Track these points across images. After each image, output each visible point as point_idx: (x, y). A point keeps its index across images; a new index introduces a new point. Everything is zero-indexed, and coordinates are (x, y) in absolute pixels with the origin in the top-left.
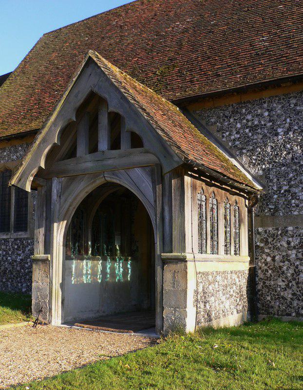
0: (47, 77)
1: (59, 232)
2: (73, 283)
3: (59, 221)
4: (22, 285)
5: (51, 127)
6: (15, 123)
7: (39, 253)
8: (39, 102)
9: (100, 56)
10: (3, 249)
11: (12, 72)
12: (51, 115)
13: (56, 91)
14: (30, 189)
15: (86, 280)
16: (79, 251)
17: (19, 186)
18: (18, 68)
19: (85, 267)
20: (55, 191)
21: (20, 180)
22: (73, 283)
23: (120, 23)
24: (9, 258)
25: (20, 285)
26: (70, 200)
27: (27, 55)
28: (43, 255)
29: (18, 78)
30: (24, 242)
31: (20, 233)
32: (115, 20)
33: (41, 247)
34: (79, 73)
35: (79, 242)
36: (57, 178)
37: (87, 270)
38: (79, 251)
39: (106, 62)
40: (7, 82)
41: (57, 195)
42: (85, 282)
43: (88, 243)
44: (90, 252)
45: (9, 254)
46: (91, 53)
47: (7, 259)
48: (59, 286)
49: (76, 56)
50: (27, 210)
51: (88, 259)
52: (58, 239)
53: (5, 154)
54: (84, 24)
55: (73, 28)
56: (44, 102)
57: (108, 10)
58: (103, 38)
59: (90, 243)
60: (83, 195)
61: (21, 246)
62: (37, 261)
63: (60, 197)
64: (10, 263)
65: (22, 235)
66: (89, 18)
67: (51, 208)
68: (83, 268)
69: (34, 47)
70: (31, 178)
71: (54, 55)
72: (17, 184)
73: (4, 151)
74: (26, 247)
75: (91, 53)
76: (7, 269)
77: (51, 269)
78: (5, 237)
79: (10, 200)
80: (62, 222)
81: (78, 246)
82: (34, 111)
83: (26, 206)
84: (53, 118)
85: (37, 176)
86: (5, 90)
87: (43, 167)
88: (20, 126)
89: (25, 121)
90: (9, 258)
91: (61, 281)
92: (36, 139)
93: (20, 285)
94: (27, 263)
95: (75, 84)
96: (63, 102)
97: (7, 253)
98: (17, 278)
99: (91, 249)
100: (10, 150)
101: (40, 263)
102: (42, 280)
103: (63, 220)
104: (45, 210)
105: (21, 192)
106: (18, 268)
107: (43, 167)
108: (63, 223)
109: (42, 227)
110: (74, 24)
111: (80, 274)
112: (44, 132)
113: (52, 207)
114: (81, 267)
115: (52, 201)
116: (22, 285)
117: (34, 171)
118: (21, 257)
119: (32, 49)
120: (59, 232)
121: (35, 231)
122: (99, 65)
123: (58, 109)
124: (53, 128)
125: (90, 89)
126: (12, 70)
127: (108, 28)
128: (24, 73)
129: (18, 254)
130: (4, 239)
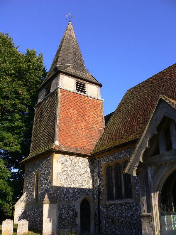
0: (133, 112)
1: (155, 198)
2: (166, 230)
3: (154, 192)
4: (132, 231)
5: (144, 139)
6: (119, 138)
7: (145, 213)
8: (130, 125)
9: (166, 97)
10: (120, 209)
11: (113, 112)
12: (143, 132)
13: (139, 118)
14: (135, 175)
15: (174, 228)
16: (167, 209)
17: (129, 173)
18: (116, 109)
19: (172, 219)
20: (150, 175)
21: (129, 170)
22: (166, 230)
23: (168, 77)
24: (124, 214)
25: (131, 230)
26: (159, 179)
27: (120, 102)
28: (147, 213)
29: (118, 115)
30: (131, 205)
31: (128, 199)
32: (165, 76)
33: (145, 208)
34: (156, 108)
35: (166, 204)
36: (150, 167)
37: (174, 222)
38: (167, 209)
39: (170, 99)
40: (112, 117)
41: (151, 177)
42: (174, 229)
43: (171, 204)
44: (174, 210)
45: (123, 212)
46: (161, 96)
47: (122, 215)
48: (159, 232)
49: (146, 98)
50: (131, 186)
51: (174, 214)
52: (155, 203)
53: (116, 155)
54: (148, 81)
55: (143, 85)
56: (133, 125)
57: (160, 71)
58: (160, 86)
59: (173, 204)
60: (167, 176)
61: (130, 207)
62: (144, 217)
63: (153, 178)
64: (124, 218)
65: (130, 200)
66: (150, 78)
67: (148, 184)
68: (171, 220)
69: (123, 98)
70: (136, 169)
71: (134, 100)
72: (128, 172)
73: (116, 154)
74: (132, 208)
75: (161, 96)
76: (123, 221)
77: (153, 221)
78: (120, 202)
79: (121, 180)
80: (156, 193)
81: (166, 206)
82: (128, 131)
83: (130, 183)
84: (144, 134)
85: (139, 167)
86: (111, 122)
87: (142, 162)
88: (122, 139)
89: (125, 137)
90: (124, 214)
91: (160, 229)
92: (136, 147)
93: (131, 230)
94: (134, 217)
95: (154, 114)
96: (148, 124)
97: (122, 212)
98: (129, 226)
99: (174, 208)
100: (118, 153)
101: (146, 218)
102: (148, 229)
103: (157, 191)
104: (145, 186)
105: (128, 176)
106: (129, 220)
107: (142, 162)
108: (156, 194)
109: (145, 196)
110: (142, 83)
111: (170, 224)
112: (140, 142)
113: (149, 184)
114: (170, 220)
115: (149, 181)
116: (132, 231)
117: (137, 164)
118: (130, 214)
119: (122, 99)
120: (155, 198)
121: (141, 199)
122: (167, 102)
123: (146, 128)
124: (145, 139)
125: (163, 115)
126: (114, 110)
127: (162, 81)
128: (120, 112)
129: (128, 212)
130: (119, 203)
